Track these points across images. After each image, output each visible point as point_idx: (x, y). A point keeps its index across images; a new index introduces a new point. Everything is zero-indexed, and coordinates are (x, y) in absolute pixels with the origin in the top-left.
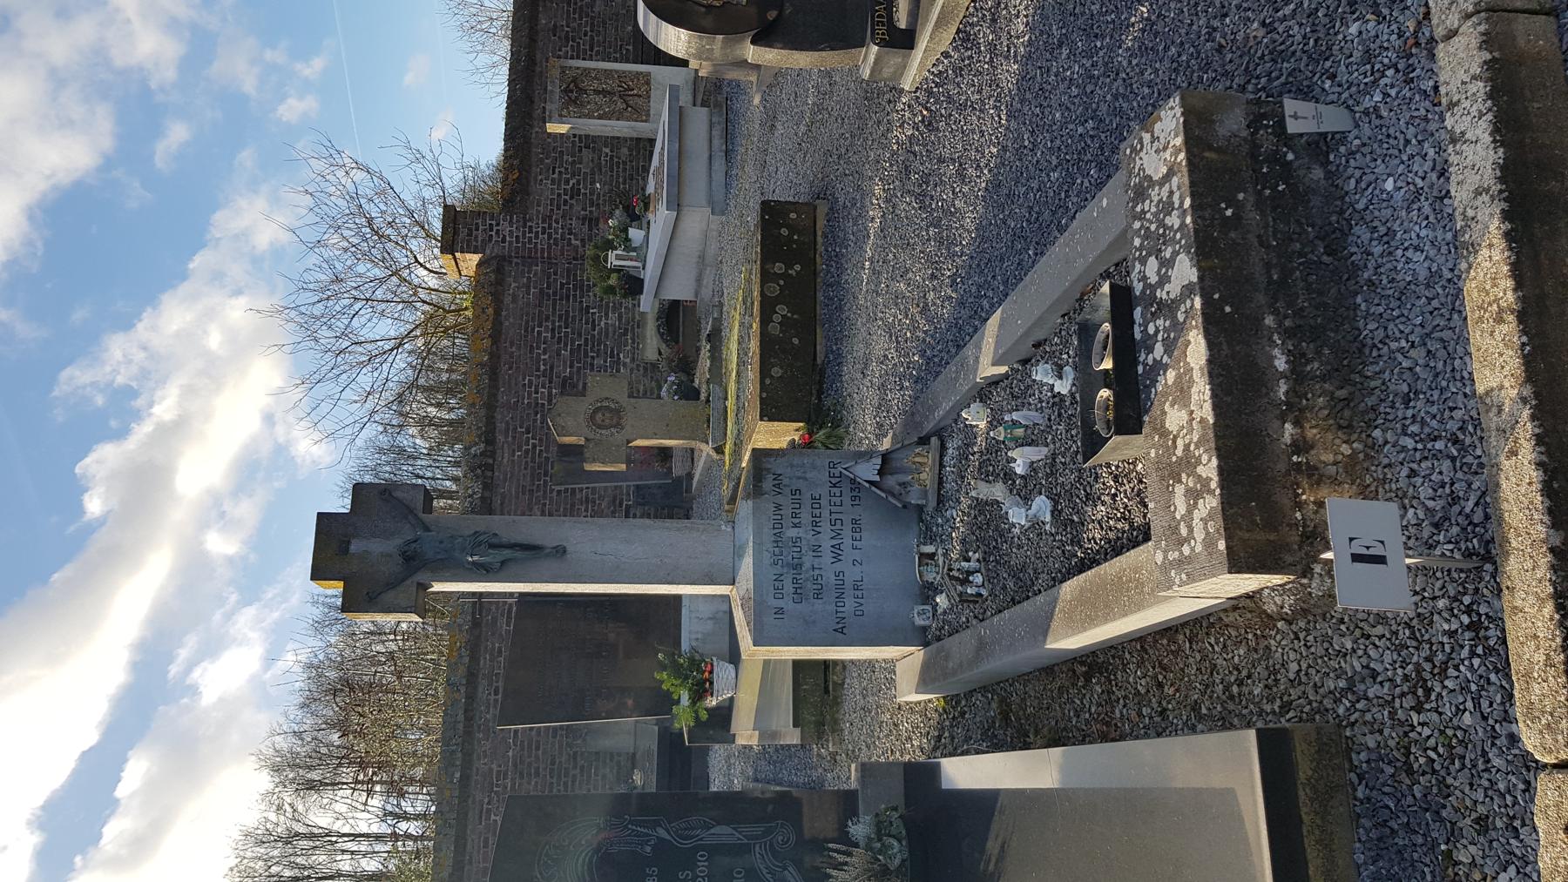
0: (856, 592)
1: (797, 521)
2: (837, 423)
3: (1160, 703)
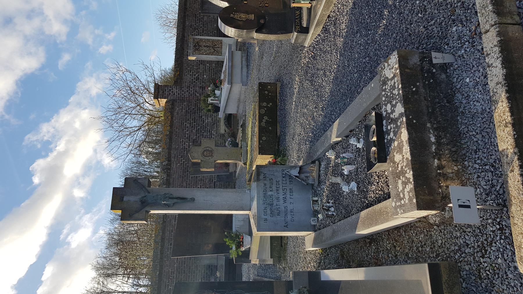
1: (271, 189)
2: (284, 155)
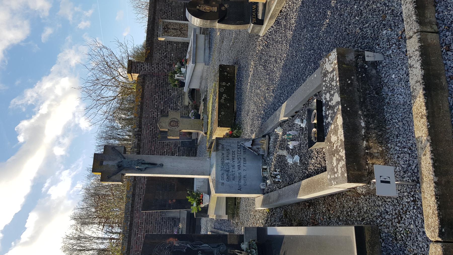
0: (244, 179)
1: (228, 158)
2: (240, 128)
3: (329, 215)
